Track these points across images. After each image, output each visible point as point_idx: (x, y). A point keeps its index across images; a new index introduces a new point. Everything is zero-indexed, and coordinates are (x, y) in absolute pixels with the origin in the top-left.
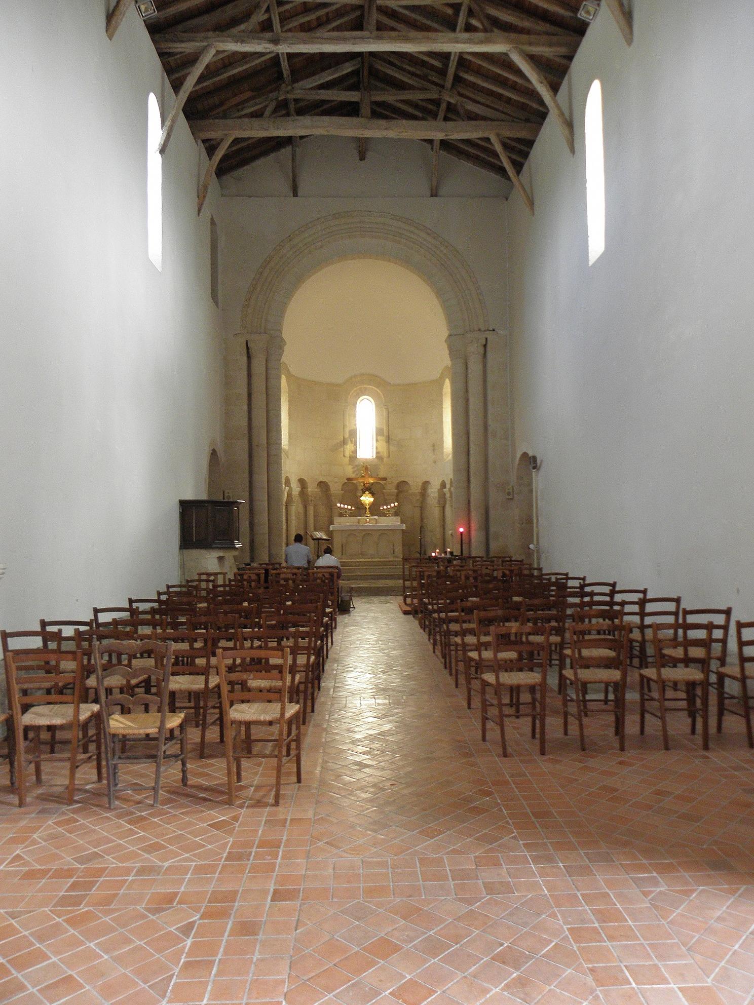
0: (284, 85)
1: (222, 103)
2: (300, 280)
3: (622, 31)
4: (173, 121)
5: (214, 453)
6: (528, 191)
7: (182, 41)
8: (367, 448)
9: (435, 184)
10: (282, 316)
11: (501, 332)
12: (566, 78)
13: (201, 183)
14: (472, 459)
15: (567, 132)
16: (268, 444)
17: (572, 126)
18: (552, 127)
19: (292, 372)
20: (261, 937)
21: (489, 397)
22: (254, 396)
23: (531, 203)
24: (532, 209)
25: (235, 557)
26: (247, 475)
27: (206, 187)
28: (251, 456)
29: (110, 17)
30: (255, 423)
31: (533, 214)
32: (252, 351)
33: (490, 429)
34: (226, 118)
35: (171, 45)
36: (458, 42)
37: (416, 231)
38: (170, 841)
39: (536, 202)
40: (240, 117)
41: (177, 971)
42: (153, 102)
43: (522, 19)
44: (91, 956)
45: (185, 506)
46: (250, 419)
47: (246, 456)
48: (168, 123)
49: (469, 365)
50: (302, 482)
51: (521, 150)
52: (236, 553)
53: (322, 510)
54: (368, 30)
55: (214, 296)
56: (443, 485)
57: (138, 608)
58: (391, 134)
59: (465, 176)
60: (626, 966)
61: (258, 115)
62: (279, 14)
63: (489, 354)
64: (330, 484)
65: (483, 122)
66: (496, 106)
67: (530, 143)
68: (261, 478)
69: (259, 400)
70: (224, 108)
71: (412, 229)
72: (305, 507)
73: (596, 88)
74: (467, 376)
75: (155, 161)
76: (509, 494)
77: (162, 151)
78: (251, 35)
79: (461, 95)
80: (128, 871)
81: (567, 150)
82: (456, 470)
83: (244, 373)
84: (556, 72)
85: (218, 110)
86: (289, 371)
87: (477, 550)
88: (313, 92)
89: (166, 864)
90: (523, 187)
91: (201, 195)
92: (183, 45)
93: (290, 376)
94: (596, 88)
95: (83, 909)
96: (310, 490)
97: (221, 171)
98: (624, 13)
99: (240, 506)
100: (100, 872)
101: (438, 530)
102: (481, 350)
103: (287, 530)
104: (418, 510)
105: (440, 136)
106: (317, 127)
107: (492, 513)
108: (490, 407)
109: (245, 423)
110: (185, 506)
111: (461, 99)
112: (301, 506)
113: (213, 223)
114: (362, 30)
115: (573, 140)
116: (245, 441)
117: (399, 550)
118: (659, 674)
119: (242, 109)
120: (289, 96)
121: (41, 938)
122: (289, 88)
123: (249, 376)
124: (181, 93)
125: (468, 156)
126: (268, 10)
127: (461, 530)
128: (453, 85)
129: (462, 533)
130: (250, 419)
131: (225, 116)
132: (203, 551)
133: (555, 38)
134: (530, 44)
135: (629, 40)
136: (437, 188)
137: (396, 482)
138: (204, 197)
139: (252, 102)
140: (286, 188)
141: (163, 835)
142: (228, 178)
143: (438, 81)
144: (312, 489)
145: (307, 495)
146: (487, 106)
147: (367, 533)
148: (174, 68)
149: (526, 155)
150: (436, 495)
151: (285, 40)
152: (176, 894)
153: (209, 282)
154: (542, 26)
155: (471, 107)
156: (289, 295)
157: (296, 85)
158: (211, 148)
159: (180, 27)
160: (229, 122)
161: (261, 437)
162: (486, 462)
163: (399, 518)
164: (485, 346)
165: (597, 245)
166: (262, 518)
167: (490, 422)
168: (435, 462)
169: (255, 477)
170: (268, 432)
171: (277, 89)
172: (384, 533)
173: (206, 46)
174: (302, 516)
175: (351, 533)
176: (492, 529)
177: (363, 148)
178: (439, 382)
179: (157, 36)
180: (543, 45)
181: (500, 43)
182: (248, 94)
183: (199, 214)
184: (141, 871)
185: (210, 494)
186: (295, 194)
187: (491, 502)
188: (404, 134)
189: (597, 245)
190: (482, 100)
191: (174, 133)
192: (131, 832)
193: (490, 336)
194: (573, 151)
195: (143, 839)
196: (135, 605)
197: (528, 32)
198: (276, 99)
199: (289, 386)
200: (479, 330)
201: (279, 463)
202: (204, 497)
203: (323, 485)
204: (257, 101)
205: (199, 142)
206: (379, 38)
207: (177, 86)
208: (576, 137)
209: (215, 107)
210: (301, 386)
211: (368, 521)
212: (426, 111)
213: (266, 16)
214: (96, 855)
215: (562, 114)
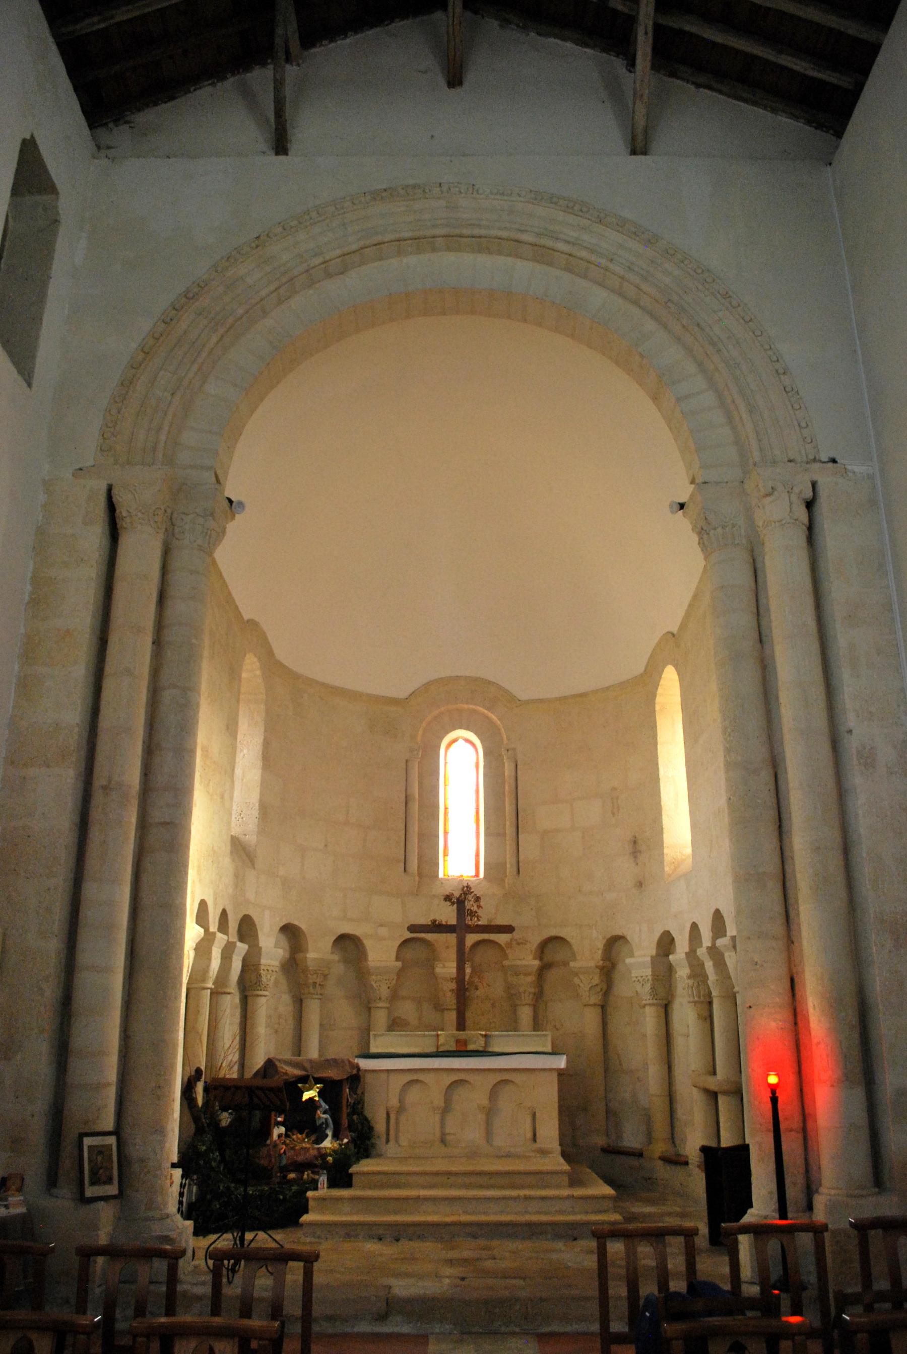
8: (462, 853)
9: (641, 122)
19: (280, 654)
32: (122, 511)
33: (852, 745)
46: (95, 711)
47: (63, 822)
64: (368, 943)
68: (112, 896)
69: (132, 651)
72: (299, 1002)
86: (270, 653)
96: (311, 955)
101: (654, 1074)
102: (802, 514)
107: (885, 1027)
109: (73, 716)
112: (287, 998)
117: (550, 1131)
127: (773, 1079)
129: (773, 1088)
130: (95, 711)
137: (536, 940)
144: (318, 951)
145: (305, 970)
150: (648, 972)
164: (810, 505)
167: (850, 719)
168: (640, 885)
169: (90, 890)
174: (289, 1026)
178: (645, 684)
203: (348, 944)
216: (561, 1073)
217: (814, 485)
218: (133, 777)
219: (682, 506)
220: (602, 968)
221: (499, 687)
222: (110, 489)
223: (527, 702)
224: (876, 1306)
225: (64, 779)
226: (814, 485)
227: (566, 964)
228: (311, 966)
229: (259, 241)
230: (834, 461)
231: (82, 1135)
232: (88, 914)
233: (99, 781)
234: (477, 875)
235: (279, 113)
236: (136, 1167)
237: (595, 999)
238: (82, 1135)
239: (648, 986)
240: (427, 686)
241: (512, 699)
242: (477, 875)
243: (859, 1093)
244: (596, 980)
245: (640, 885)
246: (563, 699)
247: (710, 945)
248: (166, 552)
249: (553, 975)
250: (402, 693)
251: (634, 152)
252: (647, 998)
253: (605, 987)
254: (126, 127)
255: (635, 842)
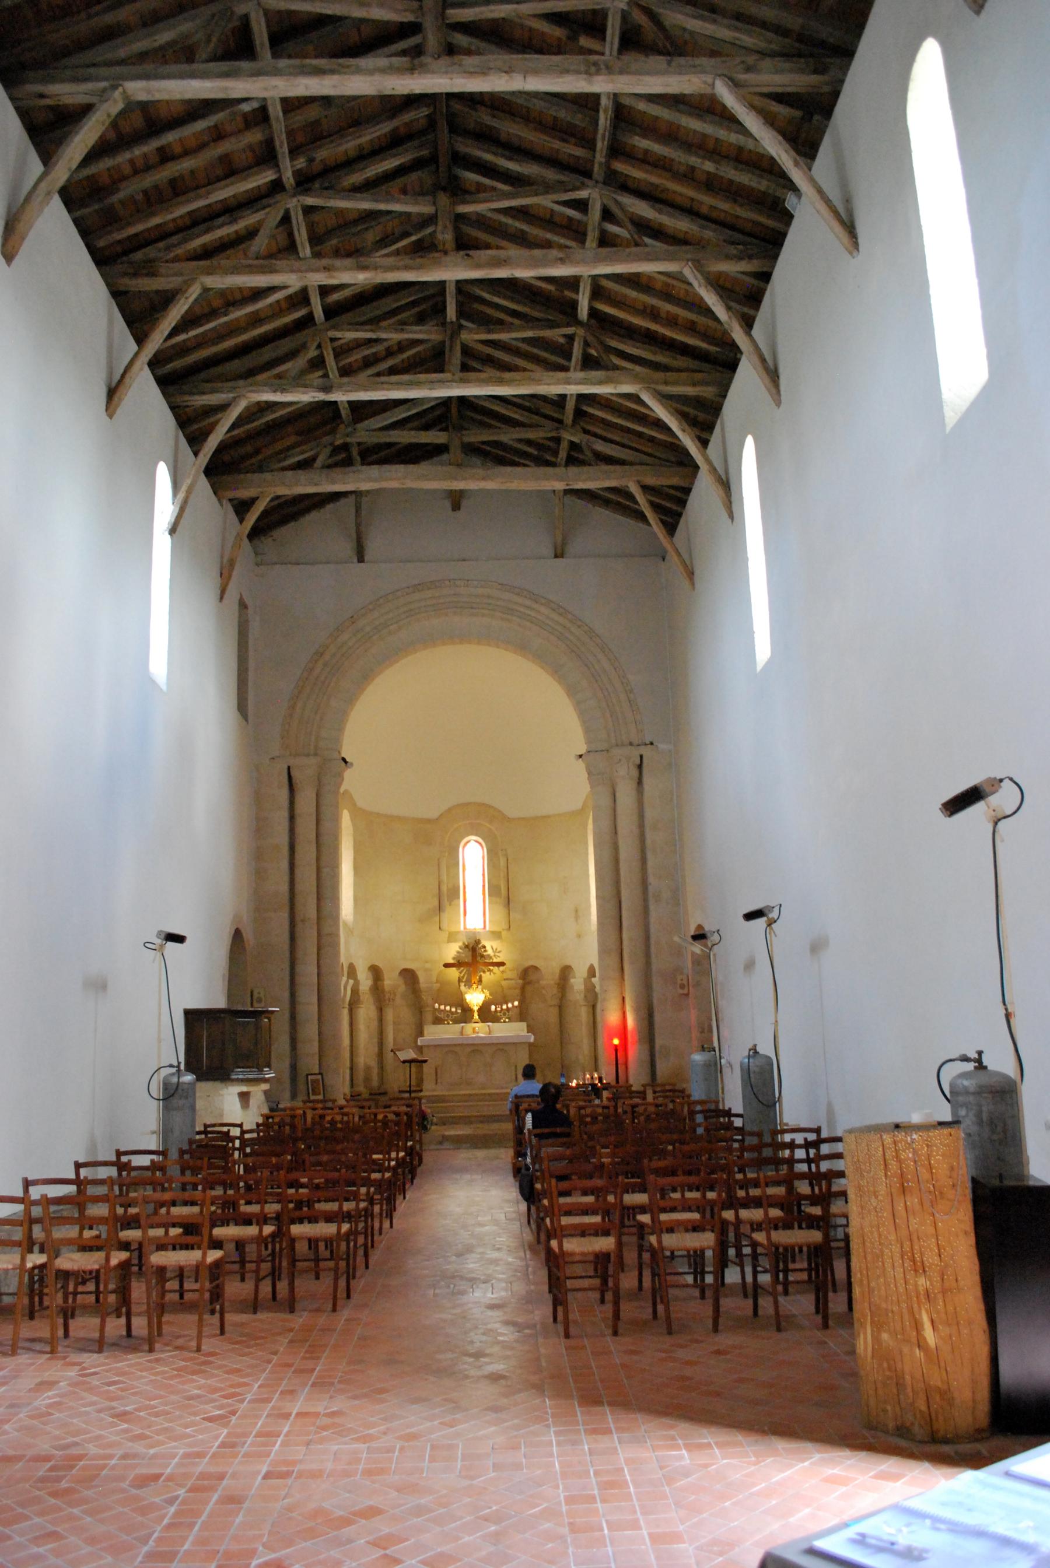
0: (342, 426)
1: (257, 451)
2: (367, 677)
3: (768, 390)
4: (189, 492)
5: (237, 935)
6: (685, 556)
7: (204, 393)
9: (559, 539)
10: (341, 729)
11: (662, 746)
12: (719, 422)
13: (225, 560)
14: (625, 936)
15: (721, 492)
16: (319, 918)
17: (727, 486)
18: (704, 487)
20: (246, 1505)
21: (648, 842)
22: (299, 848)
23: (691, 574)
24: (693, 584)
25: (266, 1092)
26: (286, 966)
27: (232, 563)
28: (293, 938)
29: (112, 393)
30: (299, 887)
31: (694, 589)
33: (651, 889)
34: (262, 472)
35: (187, 398)
36: (569, 384)
37: (536, 606)
38: (158, 1433)
39: (697, 572)
40: (284, 469)
41: (159, 1528)
42: (163, 474)
43: (655, 354)
44: (72, 1518)
45: (191, 1016)
48: (181, 495)
49: (618, 795)
50: (376, 972)
51: (671, 507)
52: (265, 1086)
53: (406, 1014)
54: (450, 371)
55: (242, 707)
56: (592, 972)
57: (130, 1161)
58: (490, 485)
59: (603, 529)
60: (607, 1522)
61: (305, 465)
62: (334, 349)
63: (646, 779)
65: (618, 468)
66: (634, 445)
67: (687, 491)
68: (308, 970)
69: (306, 853)
70: (260, 457)
71: (528, 603)
72: (380, 1010)
73: (750, 442)
74: (615, 810)
75: (162, 544)
76: (682, 987)
77: (173, 531)
78: (298, 381)
79: (586, 432)
80: (111, 1457)
81: (725, 515)
82: (603, 951)
83: (285, 814)
84: (704, 417)
85: (254, 460)
86: (354, 804)
87: (636, 1077)
88: (385, 433)
89: (152, 1451)
90: (679, 554)
91: (225, 574)
92: (204, 397)
93: (358, 813)
94: (750, 442)
95: (64, 1484)
97: (256, 533)
98: (766, 369)
99: (272, 1017)
100: (80, 1457)
102: (635, 773)
103: (352, 1046)
104: (554, 1011)
105: (560, 486)
106: (386, 480)
108: (650, 856)
109: (285, 887)
110: (191, 1016)
111: (587, 437)
113: (243, 605)
114: (442, 371)
115: (731, 503)
116: (285, 915)
118: (769, 1238)
119: (284, 459)
120: (348, 440)
121: (22, 1505)
122: (350, 429)
123: (292, 818)
124: (201, 455)
125: (606, 503)
126: (319, 346)
128: (574, 421)
129: (616, 1046)
131: (260, 469)
132: (217, 1084)
133: (699, 376)
134: (666, 383)
135: (778, 403)
136: (564, 543)
138: (230, 576)
139: (298, 450)
140: (347, 548)
141: (149, 1427)
142: (266, 543)
143: (556, 415)
144: (391, 979)
145: (383, 991)
146: (623, 446)
147: (476, 1048)
148: (192, 426)
149: (683, 503)
150: (582, 987)
151: (340, 387)
152: (162, 1474)
153: (235, 702)
154: (681, 362)
155: (600, 447)
156: (351, 700)
157: (359, 426)
158: (241, 508)
159: (203, 375)
160: (267, 476)
161: (308, 908)
162: (647, 938)
163: (524, 1025)
164: (640, 767)
165: (763, 650)
166: (310, 1031)
167: (651, 879)
168: (579, 936)
170: (318, 899)
171: (333, 431)
172: (501, 1048)
173: (235, 398)
174: (375, 1024)
175: (449, 1049)
176: (659, 1042)
177: (456, 500)
179: (171, 389)
180: (684, 384)
181: (626, 383)
182: (293, 439)
183: (221, 598)
184: (125, 1457)
185: (230, 996)
186: (361, 559)
187: (655, 1002)
188: (508, 484)
189: (763, 650)
190: (617, 438)
191: (187, 510)
192: (113, 1425)
193: (646, 751)
194: (731, 516)
195: (126, 1431)
196: (124, 1159)
197: (666, 368)
198: (331, 444)
199: (354, 825)
200: (631, 744)
201: (336, 945)
202: (220, 1002)
204: (304, 447)
205: (224, 502)
206: (463, 381)
207: (195, 441)
208: (734, 498)
209: (250, 456)
210: (372, 824)
211: (477, 1030)
212: (541, 456)
213: (316, 353)
214: (76, 1444)
215: (713, 470)
216: (530, 1045)
217: (641, 757)
218: (312, 913)
219: (581, 756)
220: (558, 984)
221: (495, 809)
222: (289, 768)
223: (514, 819)
224: (351, 982)
225: (283, 916)
226: (641, 757)
227: (538, 982)
228: (387, 988)
229: (353, 619)
230: (652, 744)
231: (307, 1075)
232: (299, 979)
233: (298, 919)
234: (485, 927)
235: (358, 525)
236: (329, 1089)
237: (555, 1002)
238: (307, 1075)
239: (582, 995)
240: (450, 810)
241: (504, 818)
242: (485, 927)
243: (646, 1047)
244: (555, 991)
245: (579, 936)
246: (536, 818)
247: (133, 1164)
248: (318, 795)
249: (528, 988)
250: (434, 814)
251: (556, 556)
252: (582, 1002)
253: (560, 995)
254: (270, 539)
255: (577, 911)
